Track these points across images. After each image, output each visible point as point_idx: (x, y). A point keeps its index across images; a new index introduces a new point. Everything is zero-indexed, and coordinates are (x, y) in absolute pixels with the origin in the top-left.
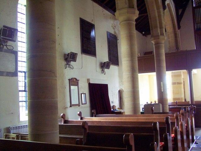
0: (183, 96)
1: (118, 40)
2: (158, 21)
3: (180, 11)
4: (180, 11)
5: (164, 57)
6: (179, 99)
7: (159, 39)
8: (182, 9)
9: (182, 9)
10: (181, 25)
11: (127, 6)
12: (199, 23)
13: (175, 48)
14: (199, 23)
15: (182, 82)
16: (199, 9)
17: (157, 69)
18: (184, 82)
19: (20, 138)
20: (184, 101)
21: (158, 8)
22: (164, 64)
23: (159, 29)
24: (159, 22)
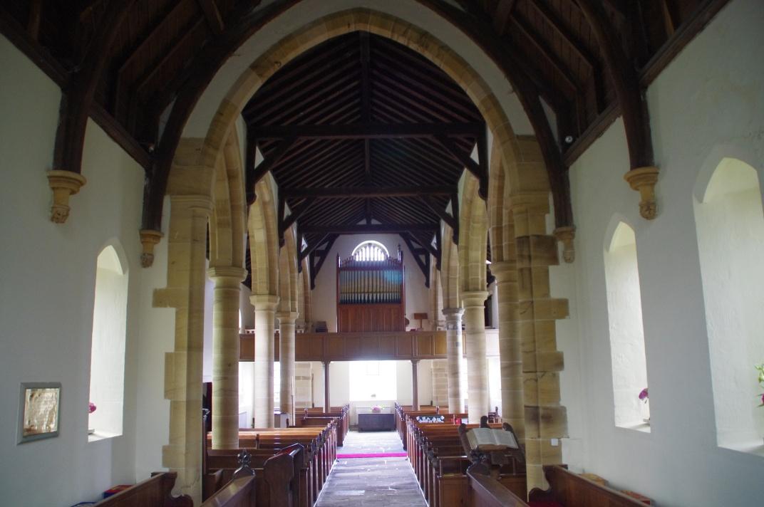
0: (310, 400)
1: (584, 471)
2: (290, 290)
3: (317, 259)
4: (317, 259)
5: (293, 344)
6: (303, 403)
7: (289, 316)
8: (90, 120)
9: (90, 120)
10: (316, 281)
11: (267, 292)
12: (386, 292)
13: (304, 320)
14: (386, 292)
15: (311, 376)
16: (382, 272)
17: (282, 357)
18: (313, 375)
19: (421, 499)
20: (311, 407)
21: (291, 272)
22: (293, 354)
23: (290, 302)
24: (291, 291)
